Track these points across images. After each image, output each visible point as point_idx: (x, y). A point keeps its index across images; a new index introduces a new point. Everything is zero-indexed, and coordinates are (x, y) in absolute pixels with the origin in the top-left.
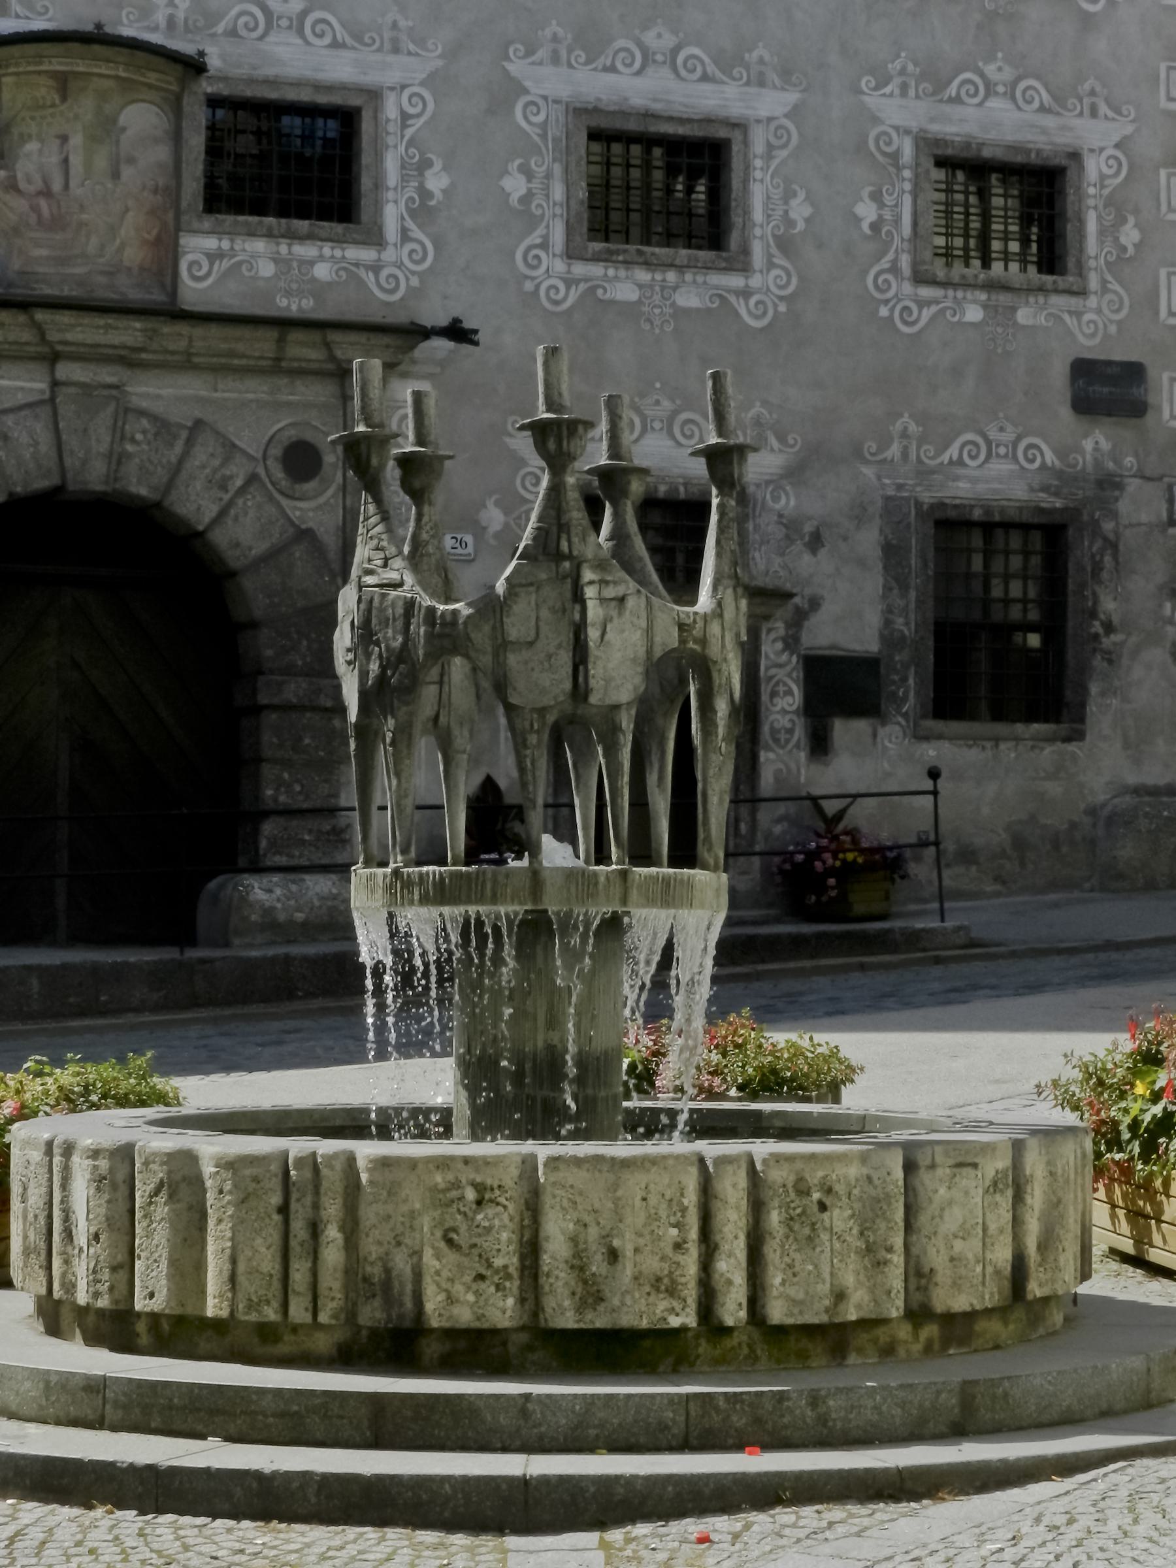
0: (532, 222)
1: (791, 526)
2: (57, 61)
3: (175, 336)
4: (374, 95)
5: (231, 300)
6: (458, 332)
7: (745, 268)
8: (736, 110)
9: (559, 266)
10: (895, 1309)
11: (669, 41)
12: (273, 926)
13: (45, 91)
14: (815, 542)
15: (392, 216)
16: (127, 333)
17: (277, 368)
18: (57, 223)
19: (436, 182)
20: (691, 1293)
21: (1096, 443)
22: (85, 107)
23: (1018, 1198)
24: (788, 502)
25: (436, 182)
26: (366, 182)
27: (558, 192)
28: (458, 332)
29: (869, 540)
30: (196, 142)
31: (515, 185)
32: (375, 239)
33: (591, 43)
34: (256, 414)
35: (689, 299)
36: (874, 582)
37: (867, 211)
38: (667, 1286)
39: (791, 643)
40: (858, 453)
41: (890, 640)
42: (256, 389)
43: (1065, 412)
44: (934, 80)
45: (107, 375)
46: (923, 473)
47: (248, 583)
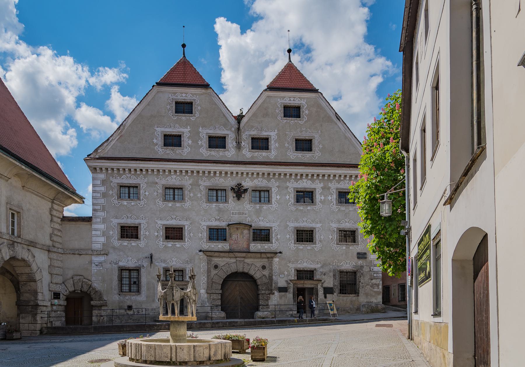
0: (290, 240)
1: (322, 273)
2: (236, 226)
3: (249, 255)
4: (271, 228)
5: (256, 251)
6: (280, 253)
7: (316, 244)
8: (314, 227)
9: (162, 243)
10: (192, 360)
11: (130, 215)
12: (260, 317)
13: (235, 229)
14: (325, 274)
15: (274, 241)
16: (244, 255)
17: (261, 258)
18: (237, 243)
19: (279, 237)
20: (169, 358)
21: (360, 262)
22: (240, 231)
23: (210, 350)
24: (321, 270)
25: (279, 237)
26: (271, 237)
27: (293, 237)
28: (280, 253)
29: (331, 274)
30: (252, 234)
31: (288, 236)
32: (272, 243)
33: (297, 220)
34: (259, 263)
35: (309, 248)
36: (332, 279)
37: (331, 237)
38: (167, 357)
39: (322, 286)
40: (330, 264)
41: (334, 285)
42: (260, 260)
43: (356, 258)
44: (339, 221)
45: (242, 259)
46: (338, 266)
47: (258, 281)
